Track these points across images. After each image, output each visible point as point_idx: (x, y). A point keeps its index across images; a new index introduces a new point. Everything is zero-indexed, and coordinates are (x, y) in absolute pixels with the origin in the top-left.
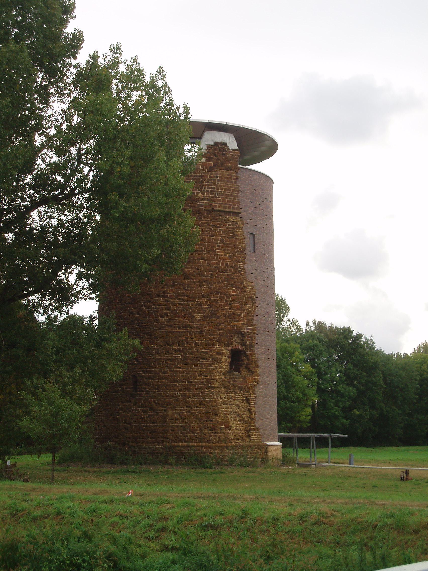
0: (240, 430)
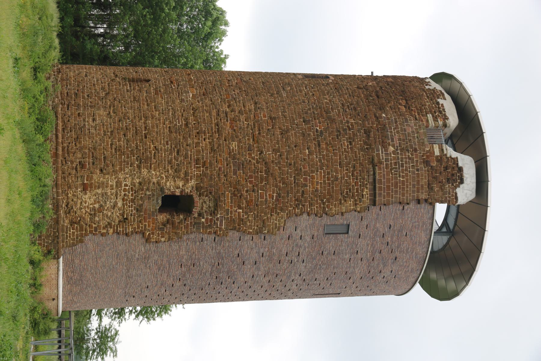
0: (81, 209)
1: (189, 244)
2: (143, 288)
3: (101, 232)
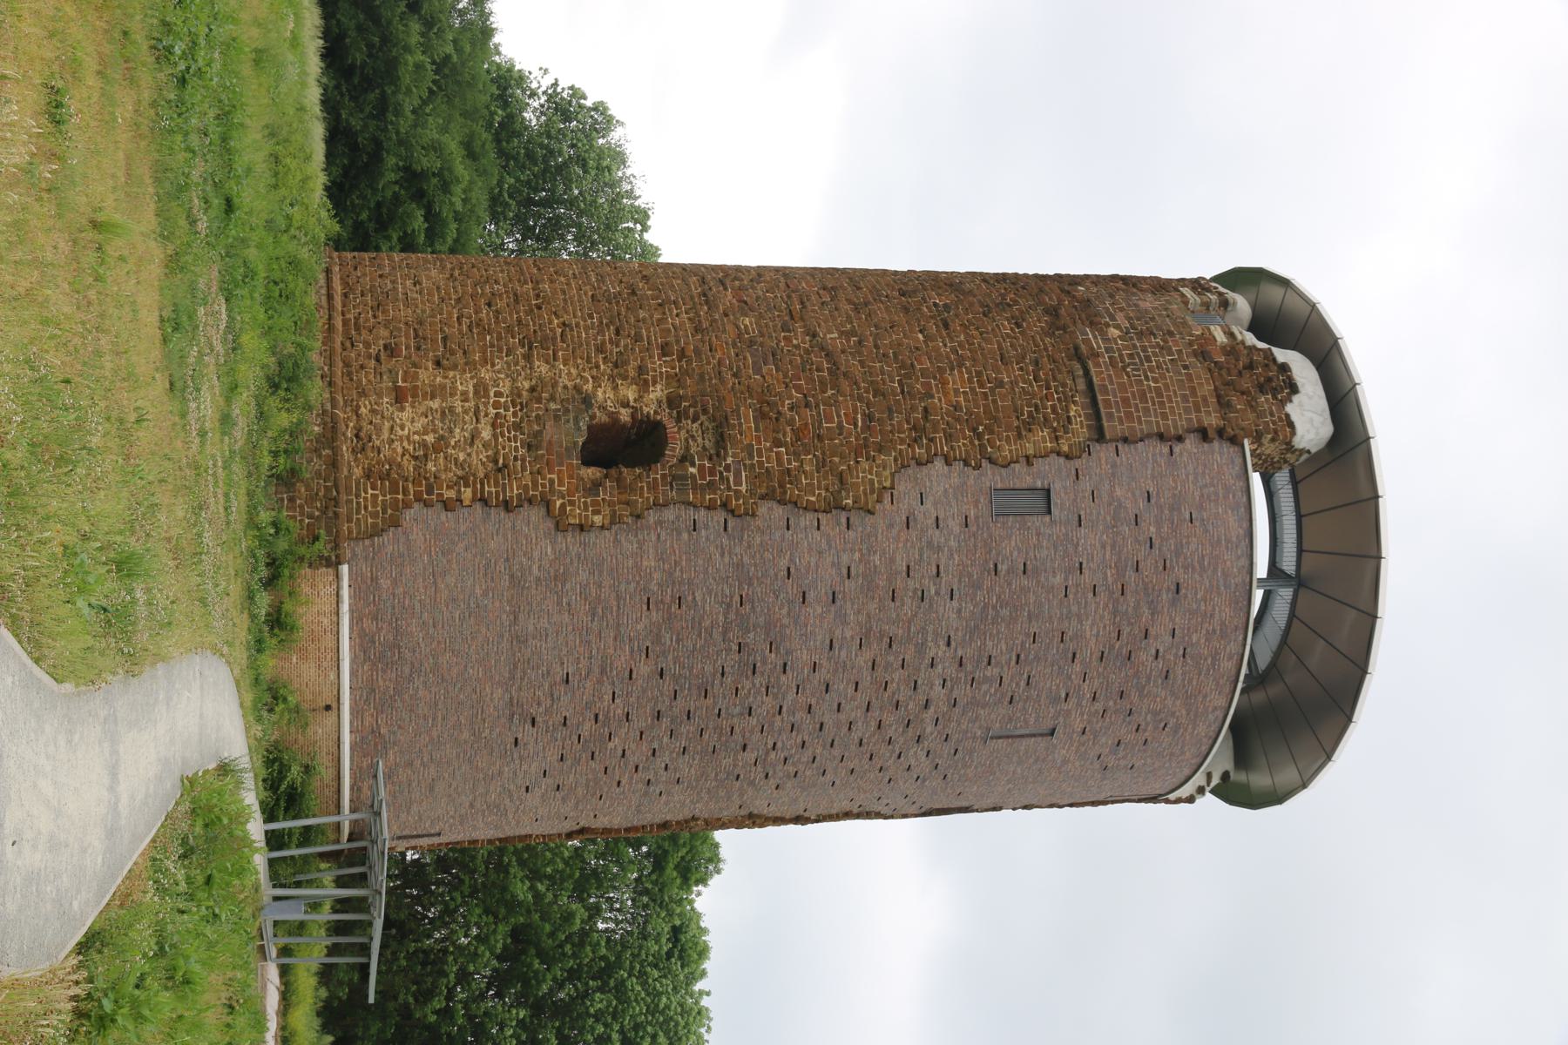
1: (662, 538)
2: (555, 683)
3: (442, 495)
